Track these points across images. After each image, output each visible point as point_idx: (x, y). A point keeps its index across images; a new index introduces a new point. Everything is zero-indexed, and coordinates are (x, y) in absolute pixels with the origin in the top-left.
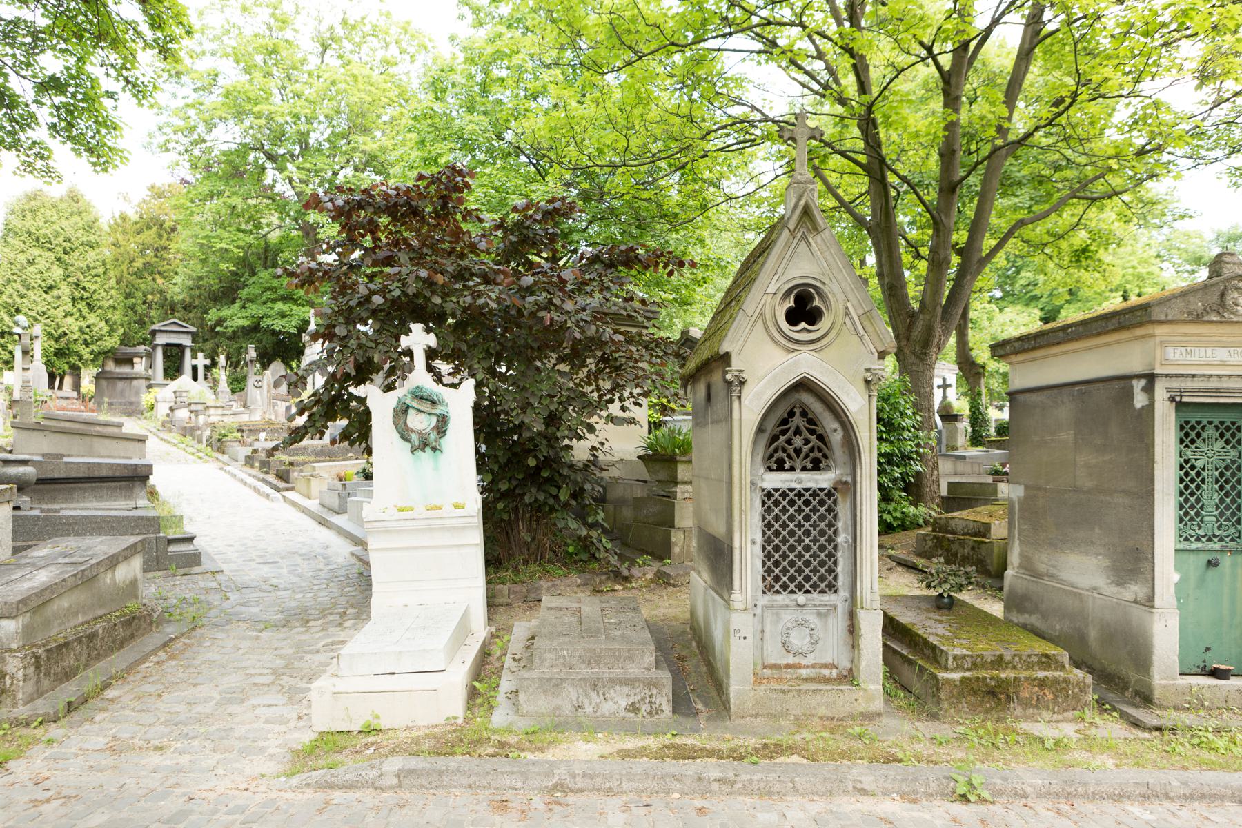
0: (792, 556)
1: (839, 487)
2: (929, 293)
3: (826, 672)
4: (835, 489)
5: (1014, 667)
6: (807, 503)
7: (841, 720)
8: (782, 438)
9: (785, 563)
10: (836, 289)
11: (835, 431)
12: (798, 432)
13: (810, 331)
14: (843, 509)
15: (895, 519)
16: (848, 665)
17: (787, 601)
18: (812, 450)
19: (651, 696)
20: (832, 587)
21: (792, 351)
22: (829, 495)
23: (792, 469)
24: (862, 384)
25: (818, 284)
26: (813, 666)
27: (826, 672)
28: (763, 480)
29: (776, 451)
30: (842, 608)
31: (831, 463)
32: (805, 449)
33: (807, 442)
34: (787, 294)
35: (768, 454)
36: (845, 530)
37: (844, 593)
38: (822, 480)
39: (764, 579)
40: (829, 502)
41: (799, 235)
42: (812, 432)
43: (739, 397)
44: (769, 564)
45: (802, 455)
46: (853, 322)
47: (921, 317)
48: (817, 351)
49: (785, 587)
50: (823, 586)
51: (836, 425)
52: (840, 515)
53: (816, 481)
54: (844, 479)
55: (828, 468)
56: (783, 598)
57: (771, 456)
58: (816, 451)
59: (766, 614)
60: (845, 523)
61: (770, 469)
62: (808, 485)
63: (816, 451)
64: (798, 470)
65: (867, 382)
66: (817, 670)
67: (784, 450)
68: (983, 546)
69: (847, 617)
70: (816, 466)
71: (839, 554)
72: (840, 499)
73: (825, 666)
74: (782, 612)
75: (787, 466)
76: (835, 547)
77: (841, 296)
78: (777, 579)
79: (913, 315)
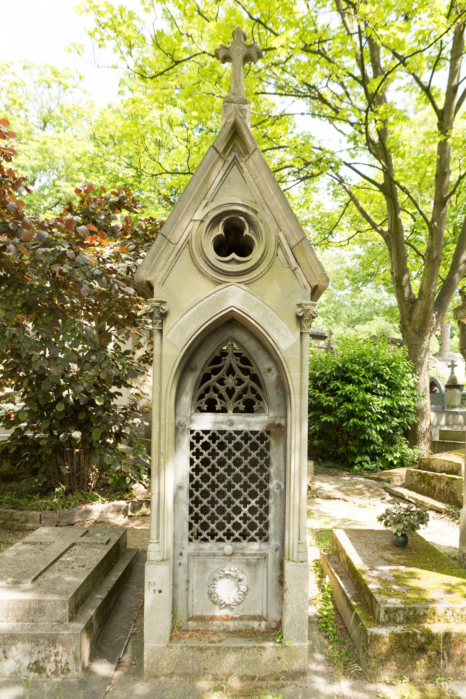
0: (221, 502)
1: (273, 430)
2: (425, 284)
3: (255, 624)
4: (268, 432)
5: (447, 621)
6: (238, 446)
7: (262, 679)
8: (214, 377)
9: (213, 510)
10: (268, 218)
11: (269, 370)
12: (231, 371)
13: (239, 262)
14: (275, 454)
15: (396, 458)
16: (277, 617)
17: (215, 550)
18: (245, 391)
19: (56, 654)
20: (263, 536)
21: (219, 283)
22: (262, 438)
23: (224, 410)
24: (293, 321)
25: (250, 213)
26: (241, 618)
27: (255, 624)
28: (191, 421)
29: (207, 390)
30: (272, 557)
31: (264, 404)
32: (238, 389)
33: (240, 382)
34: (215, 221)
35: (198, 394)
36: (278, 476)
37: (274, 542)
38: (255, 423)
39: (191, 526)
40: (262, 446)
41: (230, 159)
42: (246, 372)
43: (161, 331)
44: (197, 510)
45: (235, 396)
46: (285, 254)
47: (419, 302)
48: (247, 283)
49: (213, 535)
50: (253, 534)
51: (268, 364)
52: (272, 460)
53: (248, 424)
54: (277, 422)
55: (261, 410)
56: (210, 546)
57: (202, 396)
58: (249, 393)
59: (191, 564)
60: (278, 468)
61: (201, 410)
62: (240, 427)
63: (249, 393)
64: (230, 412)
65: (299, 319)
66: (245, 622)
67: (216, 390)
68: (454, 482)
69: (277, 566)
70: (249, 408)
71: (271, 501)
72: (273, 443)
73: (254, 618)
74: (209, 561)
75: (218, 407)
76: (267, 494)
77: (273, 226)
78: (205, 526)
79: (413, 302)
